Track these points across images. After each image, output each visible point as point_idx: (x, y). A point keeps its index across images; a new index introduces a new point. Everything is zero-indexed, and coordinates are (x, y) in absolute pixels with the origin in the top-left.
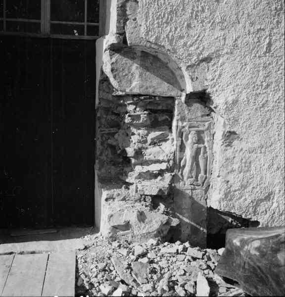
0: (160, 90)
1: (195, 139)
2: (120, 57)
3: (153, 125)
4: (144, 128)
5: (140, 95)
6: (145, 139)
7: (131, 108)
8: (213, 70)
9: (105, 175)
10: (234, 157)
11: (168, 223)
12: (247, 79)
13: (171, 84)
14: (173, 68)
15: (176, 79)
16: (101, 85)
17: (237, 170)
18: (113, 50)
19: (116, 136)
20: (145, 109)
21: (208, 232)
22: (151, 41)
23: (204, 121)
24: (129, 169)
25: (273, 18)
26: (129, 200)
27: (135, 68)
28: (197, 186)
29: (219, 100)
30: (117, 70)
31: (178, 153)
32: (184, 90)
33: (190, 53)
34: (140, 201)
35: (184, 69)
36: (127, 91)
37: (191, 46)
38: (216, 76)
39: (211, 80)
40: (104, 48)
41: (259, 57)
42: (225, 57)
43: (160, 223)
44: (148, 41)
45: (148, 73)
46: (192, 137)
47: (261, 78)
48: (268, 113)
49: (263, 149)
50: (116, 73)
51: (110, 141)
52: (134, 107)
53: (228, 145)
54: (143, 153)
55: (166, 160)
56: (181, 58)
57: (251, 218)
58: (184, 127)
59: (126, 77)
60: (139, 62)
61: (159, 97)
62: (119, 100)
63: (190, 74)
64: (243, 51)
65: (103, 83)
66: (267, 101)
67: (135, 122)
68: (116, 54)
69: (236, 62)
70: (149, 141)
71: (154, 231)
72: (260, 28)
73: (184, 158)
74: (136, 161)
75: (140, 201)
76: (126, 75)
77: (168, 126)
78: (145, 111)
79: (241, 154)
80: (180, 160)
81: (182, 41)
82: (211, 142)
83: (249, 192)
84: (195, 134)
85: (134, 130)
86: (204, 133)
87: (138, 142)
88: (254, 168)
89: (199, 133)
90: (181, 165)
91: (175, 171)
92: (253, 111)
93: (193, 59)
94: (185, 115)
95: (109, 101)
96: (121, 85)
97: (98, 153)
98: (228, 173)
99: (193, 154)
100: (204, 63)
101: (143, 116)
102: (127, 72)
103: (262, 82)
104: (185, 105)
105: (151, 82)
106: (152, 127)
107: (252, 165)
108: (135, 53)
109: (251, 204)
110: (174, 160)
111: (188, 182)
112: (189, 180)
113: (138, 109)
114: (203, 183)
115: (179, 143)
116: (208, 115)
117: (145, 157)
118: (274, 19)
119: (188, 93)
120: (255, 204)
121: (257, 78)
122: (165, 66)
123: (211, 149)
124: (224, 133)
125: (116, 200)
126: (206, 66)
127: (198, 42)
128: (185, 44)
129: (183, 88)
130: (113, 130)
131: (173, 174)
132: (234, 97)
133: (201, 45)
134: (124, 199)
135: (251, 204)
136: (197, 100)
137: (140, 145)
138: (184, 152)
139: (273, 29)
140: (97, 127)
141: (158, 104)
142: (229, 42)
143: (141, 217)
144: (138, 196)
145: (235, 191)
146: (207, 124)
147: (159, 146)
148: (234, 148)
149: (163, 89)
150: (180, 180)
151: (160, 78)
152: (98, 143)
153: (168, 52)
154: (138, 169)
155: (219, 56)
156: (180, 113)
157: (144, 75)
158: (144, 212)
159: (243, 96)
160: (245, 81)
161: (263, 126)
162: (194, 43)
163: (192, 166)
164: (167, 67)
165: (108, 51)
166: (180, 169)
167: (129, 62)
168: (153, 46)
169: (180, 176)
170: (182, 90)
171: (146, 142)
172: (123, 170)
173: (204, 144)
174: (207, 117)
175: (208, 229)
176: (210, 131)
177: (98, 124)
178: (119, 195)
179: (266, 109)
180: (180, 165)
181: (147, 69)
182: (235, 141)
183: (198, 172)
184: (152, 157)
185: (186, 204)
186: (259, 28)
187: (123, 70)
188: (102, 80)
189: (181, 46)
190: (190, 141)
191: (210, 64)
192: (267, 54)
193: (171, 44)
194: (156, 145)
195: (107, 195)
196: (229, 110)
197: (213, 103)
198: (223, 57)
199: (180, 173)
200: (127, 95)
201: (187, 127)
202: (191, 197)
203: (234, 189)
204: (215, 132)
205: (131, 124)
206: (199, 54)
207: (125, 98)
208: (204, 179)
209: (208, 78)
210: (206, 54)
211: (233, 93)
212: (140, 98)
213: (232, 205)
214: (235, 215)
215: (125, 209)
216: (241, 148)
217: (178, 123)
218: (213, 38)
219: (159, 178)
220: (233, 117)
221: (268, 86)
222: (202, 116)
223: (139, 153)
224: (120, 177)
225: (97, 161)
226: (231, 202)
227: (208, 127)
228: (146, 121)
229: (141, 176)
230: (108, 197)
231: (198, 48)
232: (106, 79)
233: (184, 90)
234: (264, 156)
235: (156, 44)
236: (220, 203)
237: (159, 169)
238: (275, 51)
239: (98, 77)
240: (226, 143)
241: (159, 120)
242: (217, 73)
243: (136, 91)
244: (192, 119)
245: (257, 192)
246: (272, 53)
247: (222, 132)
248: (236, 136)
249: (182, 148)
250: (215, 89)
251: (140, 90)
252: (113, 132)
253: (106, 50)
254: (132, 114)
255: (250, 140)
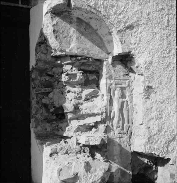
0: (92, 52)
1: (120, 94)
2: (60, 20)
3: (85, 84)
4: (79, 86)
5: (76, 56)
6: (80, 95)
7: (67, 68)
8: (135, 36)
9: (41, 132)
10: (152, 107)
11: (109, 170)
12: (157, 45)
13: (100, 48)
14: (101, 34)
15: (104, 44)
16: (38, 47)
17: (154, 117)
18: (54, 14)
19: (51, 95)
20: (79, 69)
21: (132, 174)
22: (91, 5)
23: (125, 80)
24: (65, 124)
25: (169, 2)
26: (70, 153)
27: (72, 31)
28: (123, 134)
29: (140, 60)
30: (57, 32)
31: (108, 106)
32: (110, 53)
33: (119, 20)
34: (80, 153)
35: (114, 34)
36: (66, 51)
37: (120, 14)
38: (137, 41)
39: (134, 44)
40: (44, 12)
41: (163, 29)
42: (143, 27)
43: (103, 171)
44: (89, 6)
45: (83, 37)
46: (117, 93)
47: (165, 45)
48: (171, 72)
49: (170, 100)
50: (57, 34)
51: (44, 101)
52: (71, 66)
53: (148, 98)
54: (80, 108)
55: (100, 113)
56: (113, 23)
57: (165, 157)
58: (111, 84)
59: (66, 38)
60: (75, 27)
61: (92, 58)
62: (56, 60)
63: (120, 38)
64: (154, 23)
65: (40, 46)
66: (170, 63)
67: (72, 80)
68: (56, 17)
69: (150, 31)
70: (84, 98)
71: (99, 180)
72: (162, 8)
73: (113, 110)
74: (74, 115)
75: (80, 153)
76: (65, 37)
77: (96, 85)
78: (79, 70)
79: (156, 104)
80: (111, 112)
81: (113, 10)
82: (131, 97)
83: (163, 135)
84: (120, 90)
85: (68, 88)
86: (125, 89)
87: (74, 99)
88: (165, 115)
89: (122, 89)
90: (111, 117)
91: (107, 122)
92: (162, 71)
93: (122, 26)
94: (112, 74)
95: (45, 62)
96: (62, 45)
97: (34, 112)
98: (149, 120)
99: (120, 107)
100: (128, 30)
101: (79, 75)
102: (66, 34)
103: (166, 48)
104: (111, 66)
105: (86, 44)
106: (84, 86)
107: (163, 114)
108: (72, 18)
109: (165, 145)
110: (106, 112)
111: (117, 131)
112: (118, 129)
113: (74, 69)
114: (128, 131)
115: (109, 98)
116: (127, 75)
117: (81, 111)
118: (169, 3)
119: (114, 55)
120: (167, 144)
121: (163, 45)
122: (95, 32)
123: (132, 102)
124: (144, 88)
125: (59, 154)
126: (130, 32)
127: (124, 12)
128: (115, 13)
129: (109, 52)
130: (47, 90)
131: (106, 125)
132: (150, 59)
133: (127, 15)
134: (67, 153)
135: (165, 145)
136: (119, 62)
137: (77, 101)
138: (112, 105)
139: (169, 10)
140: (31, 88)
141: (89, 65)
142: (145, 15)
143: (88, 167)
144: (78, 148)
145: (154, 135)
146: (127, 82)
147: (91, 101)
148: (152, 100)
149: (94, 52)
150: (111, 130)
151: (92, 42)
152: (34, 102)
153: (104, 18)
154: (74, 124)
155: (138, 25)
156: (108, 73)
157: (80, 38)
158: (90, 162)
159: (155, 59)
160: (156, 47)
161: (168, 82)
162: (121, 12)
163: (119, 117)
164: (97, 34)
165: (50, 13)
166: (110, 120)
167: (68, 26)
168: (92, 10)
169: (111, 126)
170: (109, 54)
171: (80, 98)
172: (58, 126)
173: (125, 98)
174: (127, 77)
175: (132, 171)
176: (129, 88)
177: (32, 85)
178: (61, 149)
179: (170, 69)
180: (110, 117)
181: (82, 33)
182: (152, 94)
183: (123, 123)
184: (88, 111)
185: (116, 151)
186: (162, 7)
187: (63, 32)
188: (39, 43)
189: (112, 14)
190: (116, 96)
191: (133, 31)
192: (168, 28)
193: (106, 11)
194: (89, 100)
195: (51, 150)
196: (148, 69)
197: (135, 63)
198: (141, 26)
199: (111, 123)
200: (66, 56)
201: (114, 84)
202: (120, 145)
203: (153, 134)
204: (133, 89)
205: (67, 82)
206: (126, 22)
207: (62, 59)
208: (128, 128)
209: (132, 42)
210: (130, 23)
211: (149, 55)
212: (78, 58)
213: (153, 147)
214: (155, 155)
215: (72, 161)
216: (156, 99)
217: (107, 80)
218: (134, 11)
219: (94, 130)
220: (150, 74)
221: (170, 51)
222: (124, 75)
223: (77, 108)
224: (56, 132)
225: (33, 120)
226: (152, 145)
227: (128, 85)
228: (82, 79)
229: (79, 129)
230: (52, 152)
231: (125, 17)
232: (43, 42)
233: (110, 53)
234: (170, 105)
235: (95, 9)
236: (145, 146)
237: (95, 122)
238: (171, 26)
239: (34, 40)
240: (146, 96)
241: (90, 79)
242: (138, 39)
243: (75, 52)
244: (117, 77)
245: (168, 135)
246: (170, 27)
247: (143, 87)
248: (152, 90)
249: (111, 102)
250: (137, 52)
251: (77, 51)
252: (47, 91)
253: (47, 13)
254: (70, 72)
255: (161, 93)
